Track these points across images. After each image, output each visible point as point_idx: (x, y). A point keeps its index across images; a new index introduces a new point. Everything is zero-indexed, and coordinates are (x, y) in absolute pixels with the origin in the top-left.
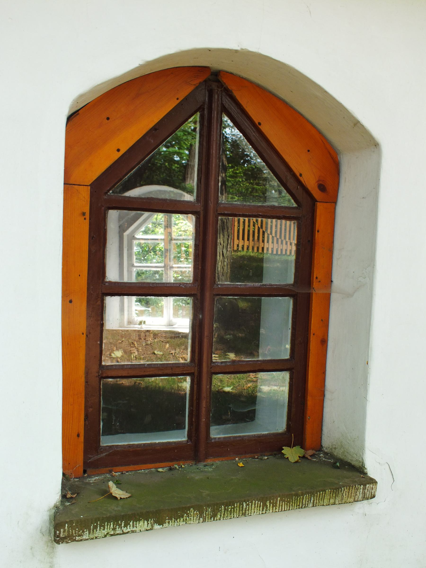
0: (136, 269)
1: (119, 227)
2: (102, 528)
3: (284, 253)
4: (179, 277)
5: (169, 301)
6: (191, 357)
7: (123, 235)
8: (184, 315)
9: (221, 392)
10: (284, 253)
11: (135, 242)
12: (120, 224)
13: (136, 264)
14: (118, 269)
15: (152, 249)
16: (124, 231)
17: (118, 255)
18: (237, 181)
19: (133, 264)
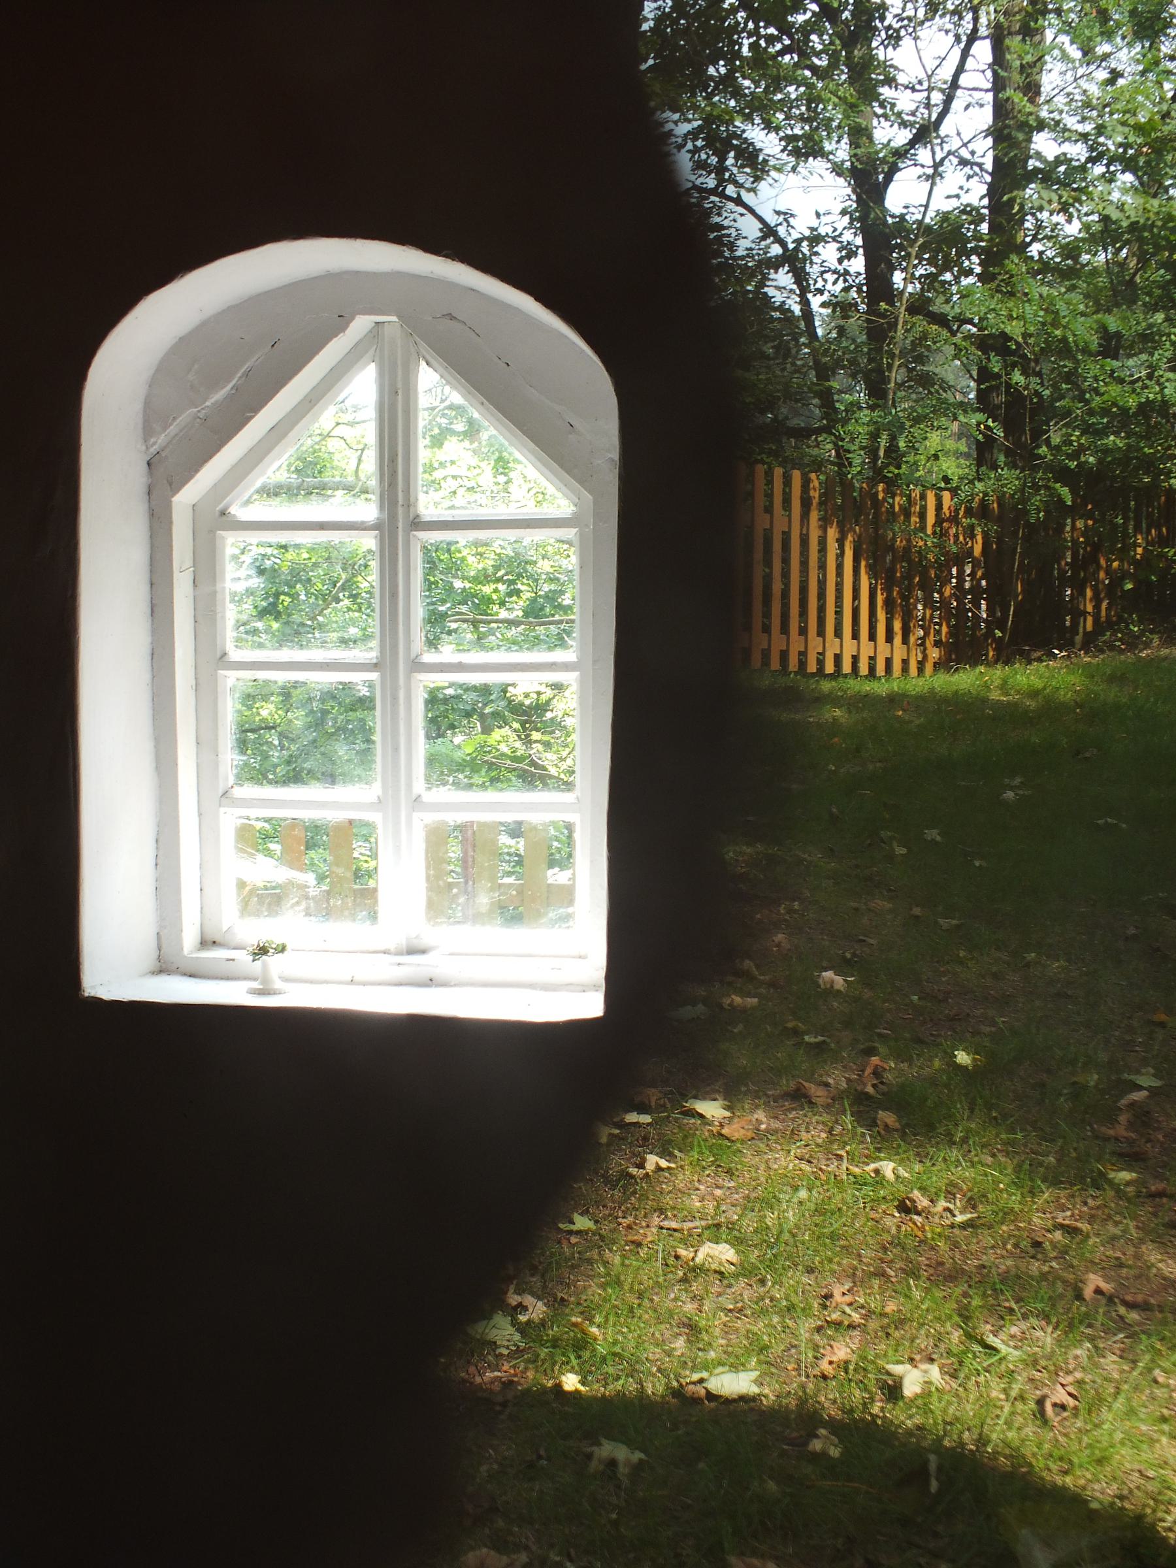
1: (149, 464)
2: (874, 104)
3: (847, 668)
6: (552, 477)
7: (171, 502)
9: (695, 1400)
10: (847, 668)
11: (231, 542)
13: (235, 655)
14: (146, 676)
16: (176, 485)
17: (143, 607)
19: (225, 654)
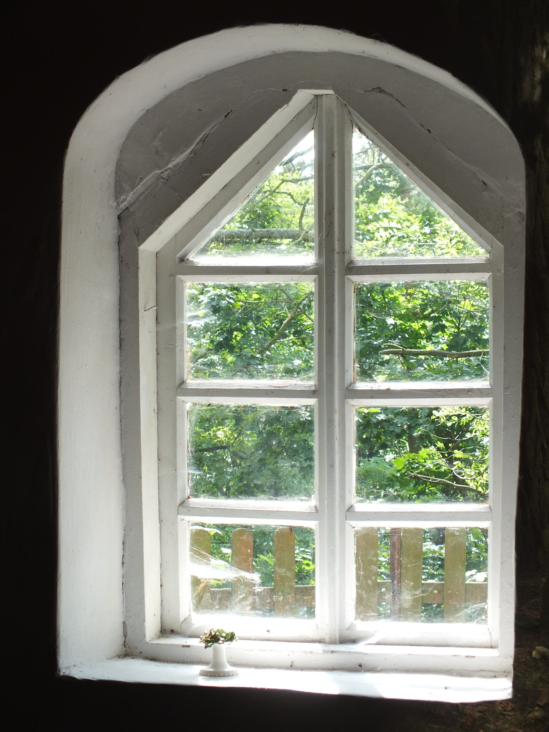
0: (195, 404)
1: (119, 217)
4: (377, 413)
5: (337, 569)
7: (137, 250)
8: (406, 605)
12: (123, 206)
13: (192, 383)
14: (114, 401)
15: (289, 325)
17: (112, 342)
18: (427, 290)
19: (183, 382)
